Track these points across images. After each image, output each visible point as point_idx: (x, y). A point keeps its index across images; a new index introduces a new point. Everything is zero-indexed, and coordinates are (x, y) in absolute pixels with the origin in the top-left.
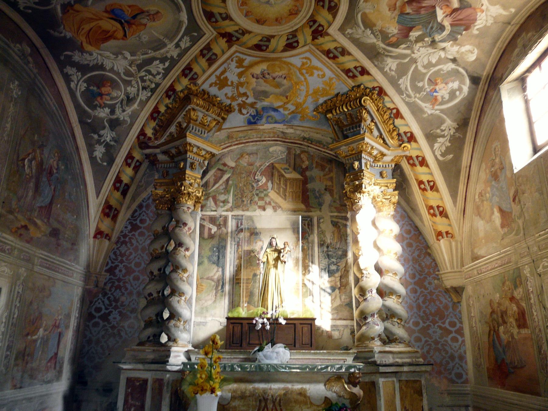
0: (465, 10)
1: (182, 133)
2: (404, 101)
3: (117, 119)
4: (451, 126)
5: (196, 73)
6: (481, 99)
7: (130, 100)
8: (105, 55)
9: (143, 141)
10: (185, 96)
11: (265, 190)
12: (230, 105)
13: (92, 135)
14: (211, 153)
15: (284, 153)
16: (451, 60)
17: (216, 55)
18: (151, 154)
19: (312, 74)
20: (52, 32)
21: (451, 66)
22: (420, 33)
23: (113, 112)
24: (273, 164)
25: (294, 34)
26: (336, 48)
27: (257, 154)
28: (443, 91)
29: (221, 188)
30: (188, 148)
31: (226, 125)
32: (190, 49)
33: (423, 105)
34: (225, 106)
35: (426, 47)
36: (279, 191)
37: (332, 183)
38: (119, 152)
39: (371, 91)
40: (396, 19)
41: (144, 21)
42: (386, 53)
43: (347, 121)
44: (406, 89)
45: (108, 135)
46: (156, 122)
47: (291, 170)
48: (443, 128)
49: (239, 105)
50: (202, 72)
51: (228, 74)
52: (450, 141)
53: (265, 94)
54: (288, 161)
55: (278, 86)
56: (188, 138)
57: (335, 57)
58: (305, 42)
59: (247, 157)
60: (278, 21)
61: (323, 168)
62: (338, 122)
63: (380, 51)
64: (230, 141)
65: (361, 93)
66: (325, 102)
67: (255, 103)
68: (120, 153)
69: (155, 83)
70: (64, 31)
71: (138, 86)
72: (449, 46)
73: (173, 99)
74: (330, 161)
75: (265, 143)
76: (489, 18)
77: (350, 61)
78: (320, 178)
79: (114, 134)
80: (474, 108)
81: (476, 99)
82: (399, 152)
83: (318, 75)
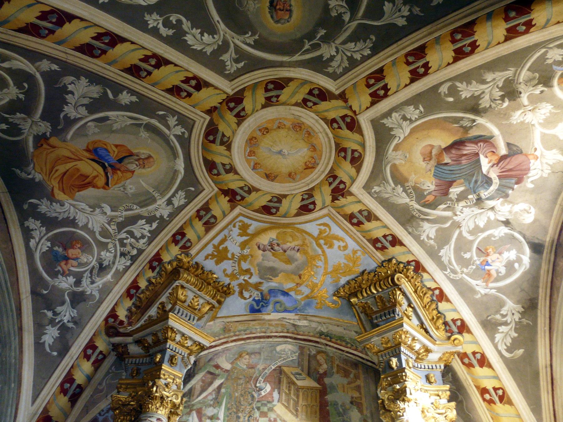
0: (516, 156)
1: (164, 316)
2: (448, 278)
3: (83, 293)
4: (514, 309)
5: (189, 240)
6: (548, 271)
7: (102, 269)
8: (80, 207)
9: (112, 326)
10: (173, 269)
11: (269, 402)
12: (229, 284)
13: (46, 311)
14: (200, 344)
15: (295, 353)
16: (502, 222)
17: (214, 217)
18: (121, 344)
19: (331, 246)
20: (18, 171)
21: (503, 230)
22: (462, 189)
23: (78, 283)
24: (280, 367)
25: (310, 194)
26: (360, 212)
27: (260, 353)
28: (497, 264)
29: (210, 398)
30: (170, 334)
31: (223, 312)
32: (185, 207)
33: (473, 282)
34: (223, 286)
35: (470, 207)
36: (289, 404)
37: (360, 394)
38: (77, 338)
39: (405, 267)
40: (433, 171)
41: (132, 167)
42: (422, 217)
43: (377, 305)
44: (450, 262)
45: (66, 313)
46: (132, 301)
47: (304, 376)
48: (503, 312)
49: (240, 285)
50: (196, 238)
51: (230, 243)
52: (516, 330)
53: (273, 272)
54: (300, 364)
55: (289, 261)
56: (170, 320)
57: (359, 223)
58: (324, 203)
59: (247, 357)
60: (291, 176)
61: (346, 374)
62: (366, 310)
63: (414, 213)
64: (227, 335)
65: (393, 269)
66: (348, 283)
67: (260, 283)
68: (79, 339)
69: (137, 249)
70: (33, 172)
71: (116, 251)
72: (499, 205)
73: (158, 273)
74: (355, 365)
75: (271, 340)
76: (546, 166)
77: (377, 228)
78: (344, 387)
79: (74, 313)
80: (541, 285)
81: (542, 272)
82: (449, 347)
83: (339, 247)
